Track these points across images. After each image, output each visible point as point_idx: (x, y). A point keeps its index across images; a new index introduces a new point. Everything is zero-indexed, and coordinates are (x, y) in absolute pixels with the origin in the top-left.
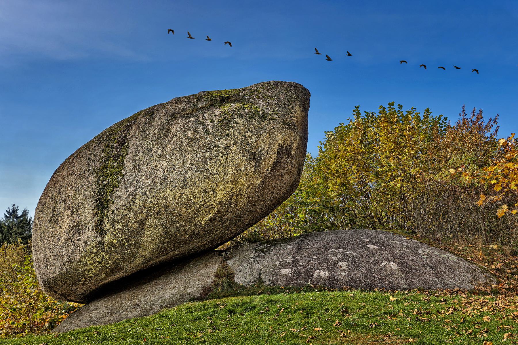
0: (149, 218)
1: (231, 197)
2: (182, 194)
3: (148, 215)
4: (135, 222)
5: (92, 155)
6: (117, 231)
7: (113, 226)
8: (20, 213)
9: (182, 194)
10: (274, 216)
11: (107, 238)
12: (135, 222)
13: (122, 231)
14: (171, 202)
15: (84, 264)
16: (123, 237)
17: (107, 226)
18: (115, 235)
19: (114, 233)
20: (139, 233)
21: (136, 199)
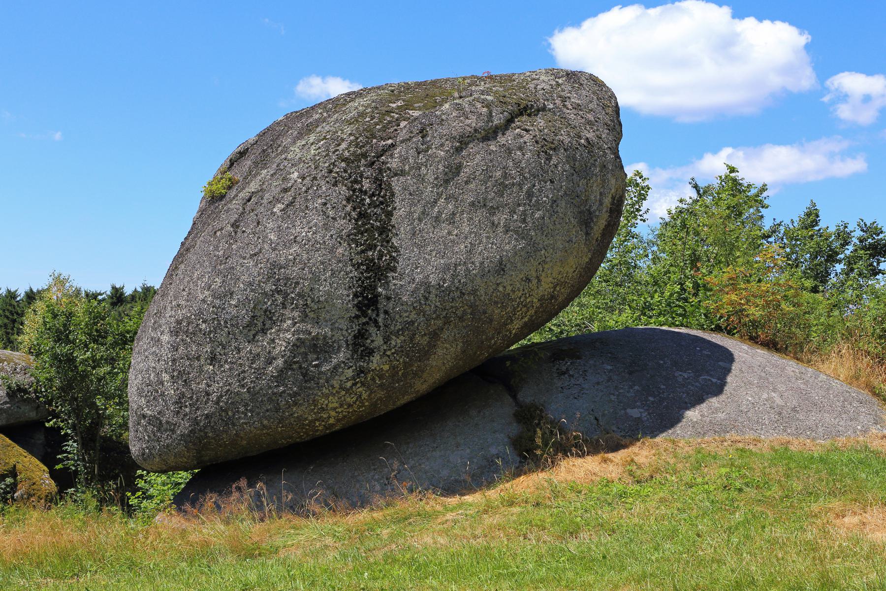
0: (446, 326)
1: (555, 288)
2: (498, 284)
3: (447, 322)
4: (425, 334)
5: (328, 206)
6: (393, 351)
7: (387, 340)
8: (56, 275)
9: (498, 284)
10: (581, 305)
11: (376, 362)
12: (425, 334)
13: (401, 351)
14: (482, 298)
15: (322, 408)
16: (401, 360)
17: (376, 339)
18: (389, 356)
19: (388, 353)
20: (425, 353)
21: (429, 293)
